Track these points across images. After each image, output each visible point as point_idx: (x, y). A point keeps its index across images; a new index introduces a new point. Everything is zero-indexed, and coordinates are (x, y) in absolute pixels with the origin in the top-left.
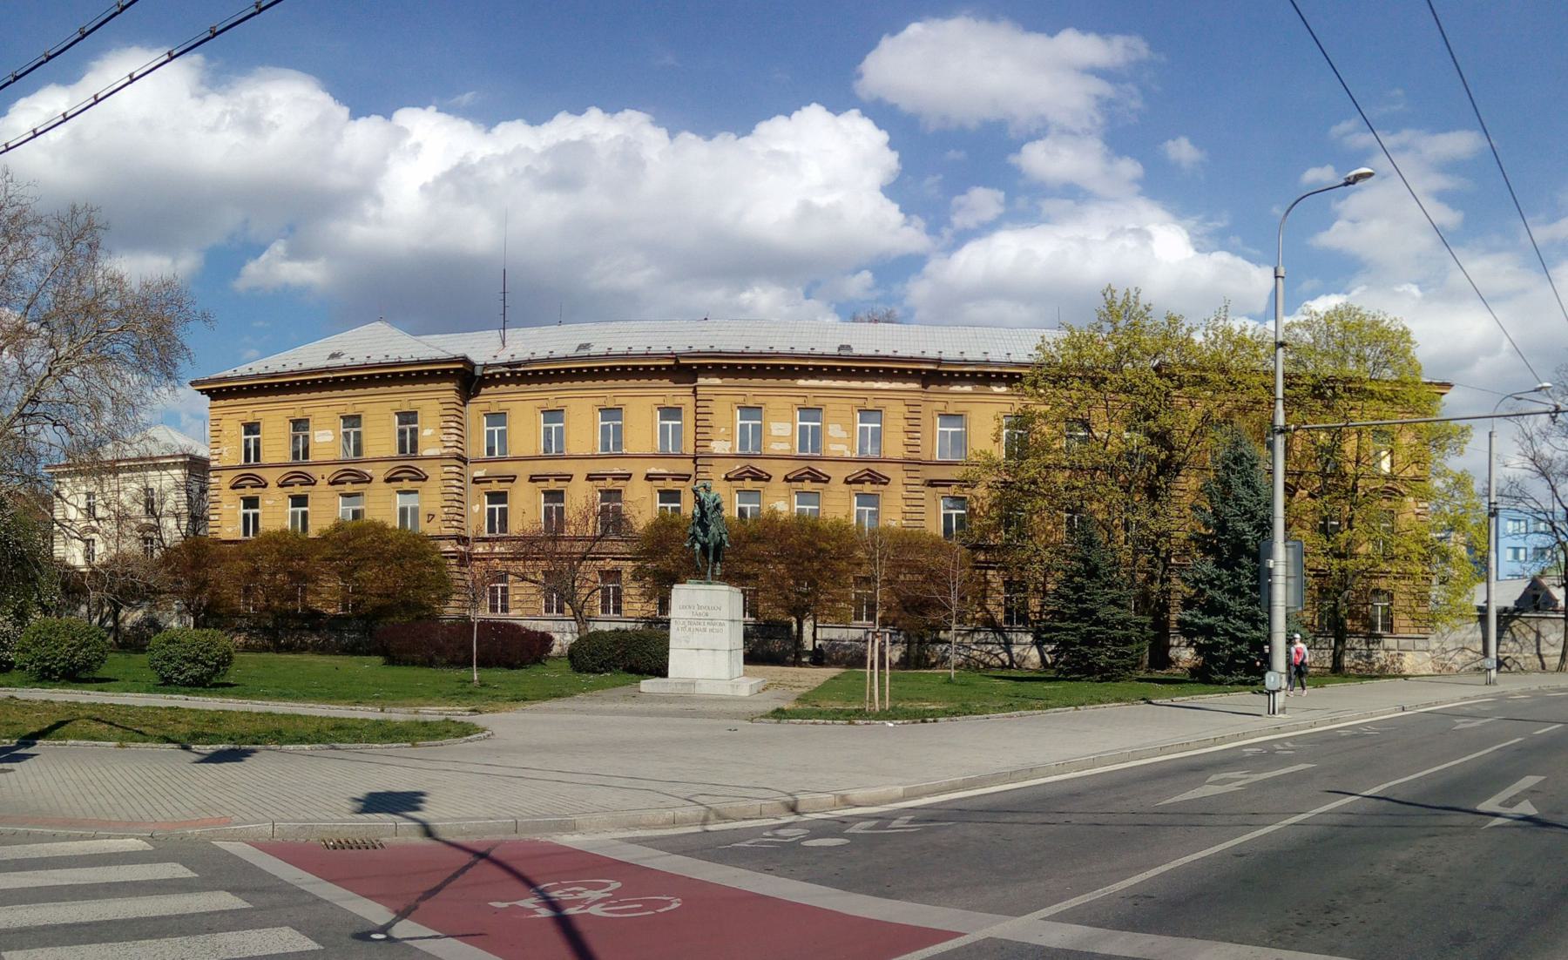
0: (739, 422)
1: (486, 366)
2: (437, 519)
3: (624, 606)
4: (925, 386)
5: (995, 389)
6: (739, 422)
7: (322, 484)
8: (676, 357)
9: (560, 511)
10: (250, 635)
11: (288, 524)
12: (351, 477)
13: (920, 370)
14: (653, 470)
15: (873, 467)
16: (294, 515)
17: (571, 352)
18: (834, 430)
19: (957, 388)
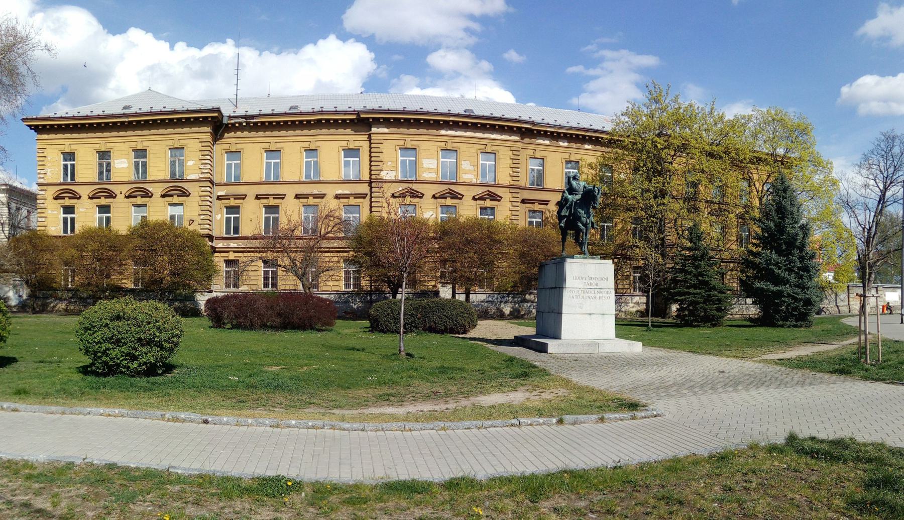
0: (400, 158)
1: (230, 117)
2: (195, 223)
3: (279, 282)
4: (522, 139)
5: (561, 144)
6: (400, 158)
7: (120, 198)
8: (358, 113)
9: (276, 220)
10: (70, 302)
11: (96, 224)
12: (139, 193)
13: (522, 128)
14: (340, 192)
15: (492, 189)
16: (101, 219)
17: (119, 111)
18: (465, 165)
19: (540, 141)
